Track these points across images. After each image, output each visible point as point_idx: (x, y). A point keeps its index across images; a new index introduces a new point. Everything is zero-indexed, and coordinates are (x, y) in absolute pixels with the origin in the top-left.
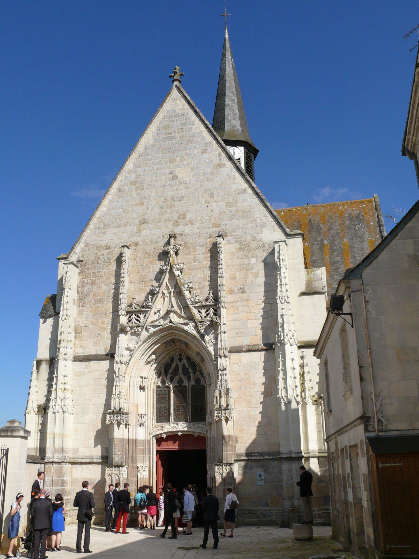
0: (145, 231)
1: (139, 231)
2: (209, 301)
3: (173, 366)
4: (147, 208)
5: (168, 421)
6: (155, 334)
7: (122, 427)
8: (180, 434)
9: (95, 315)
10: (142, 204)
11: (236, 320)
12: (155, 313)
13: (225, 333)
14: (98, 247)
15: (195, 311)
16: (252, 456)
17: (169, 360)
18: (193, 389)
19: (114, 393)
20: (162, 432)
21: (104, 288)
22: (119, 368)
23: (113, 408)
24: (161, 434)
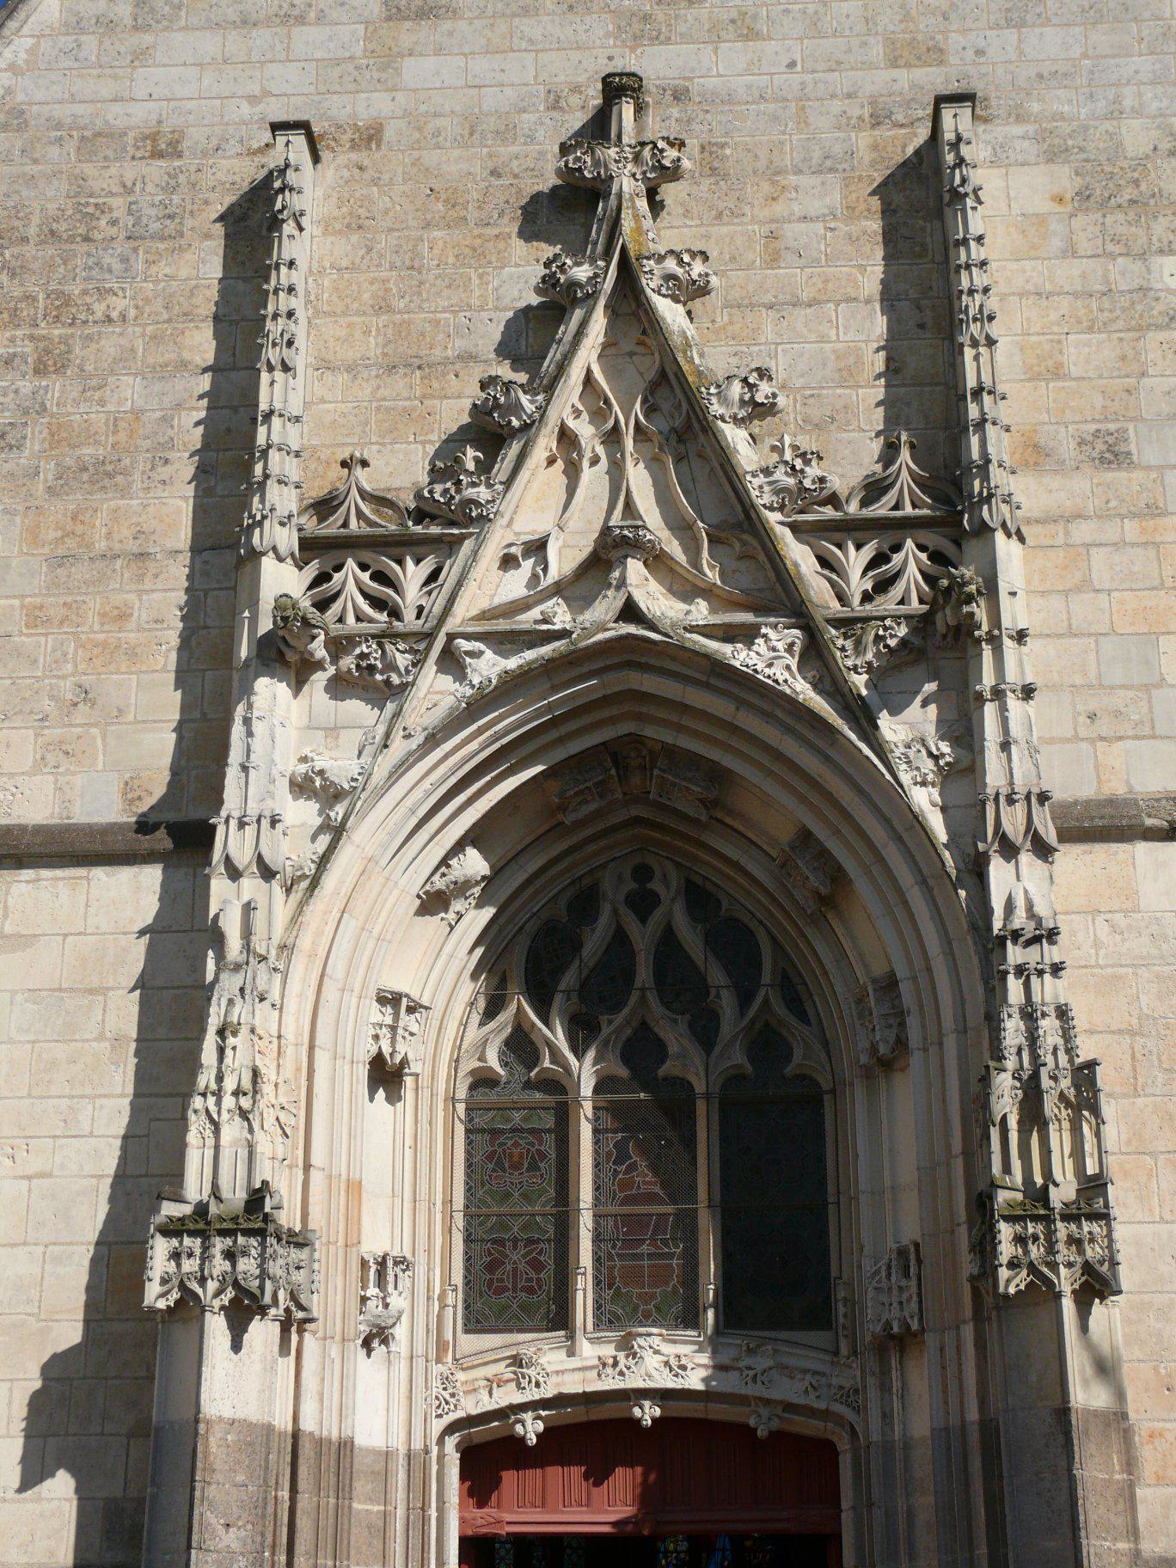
0: (430, 62)
1: (387, 60)
2: (890, 497)
3: (594, 942)
5: (560, 1320)
6: (510, 688)
7: (262, 1332)
8: (648, 1413)
9: (62, 561)
11: (1071, 633)
12: (508, 562)
13: (1028, 692)
14: (95, 141)
15: (799, 556)
17: (563, 902)
18: (735, 1102)
19: (206, 1078)
20: (518, 1398)
21: (129, 391)
22: (248, 908)
23: (195, 1187)
24: (502, 1414)
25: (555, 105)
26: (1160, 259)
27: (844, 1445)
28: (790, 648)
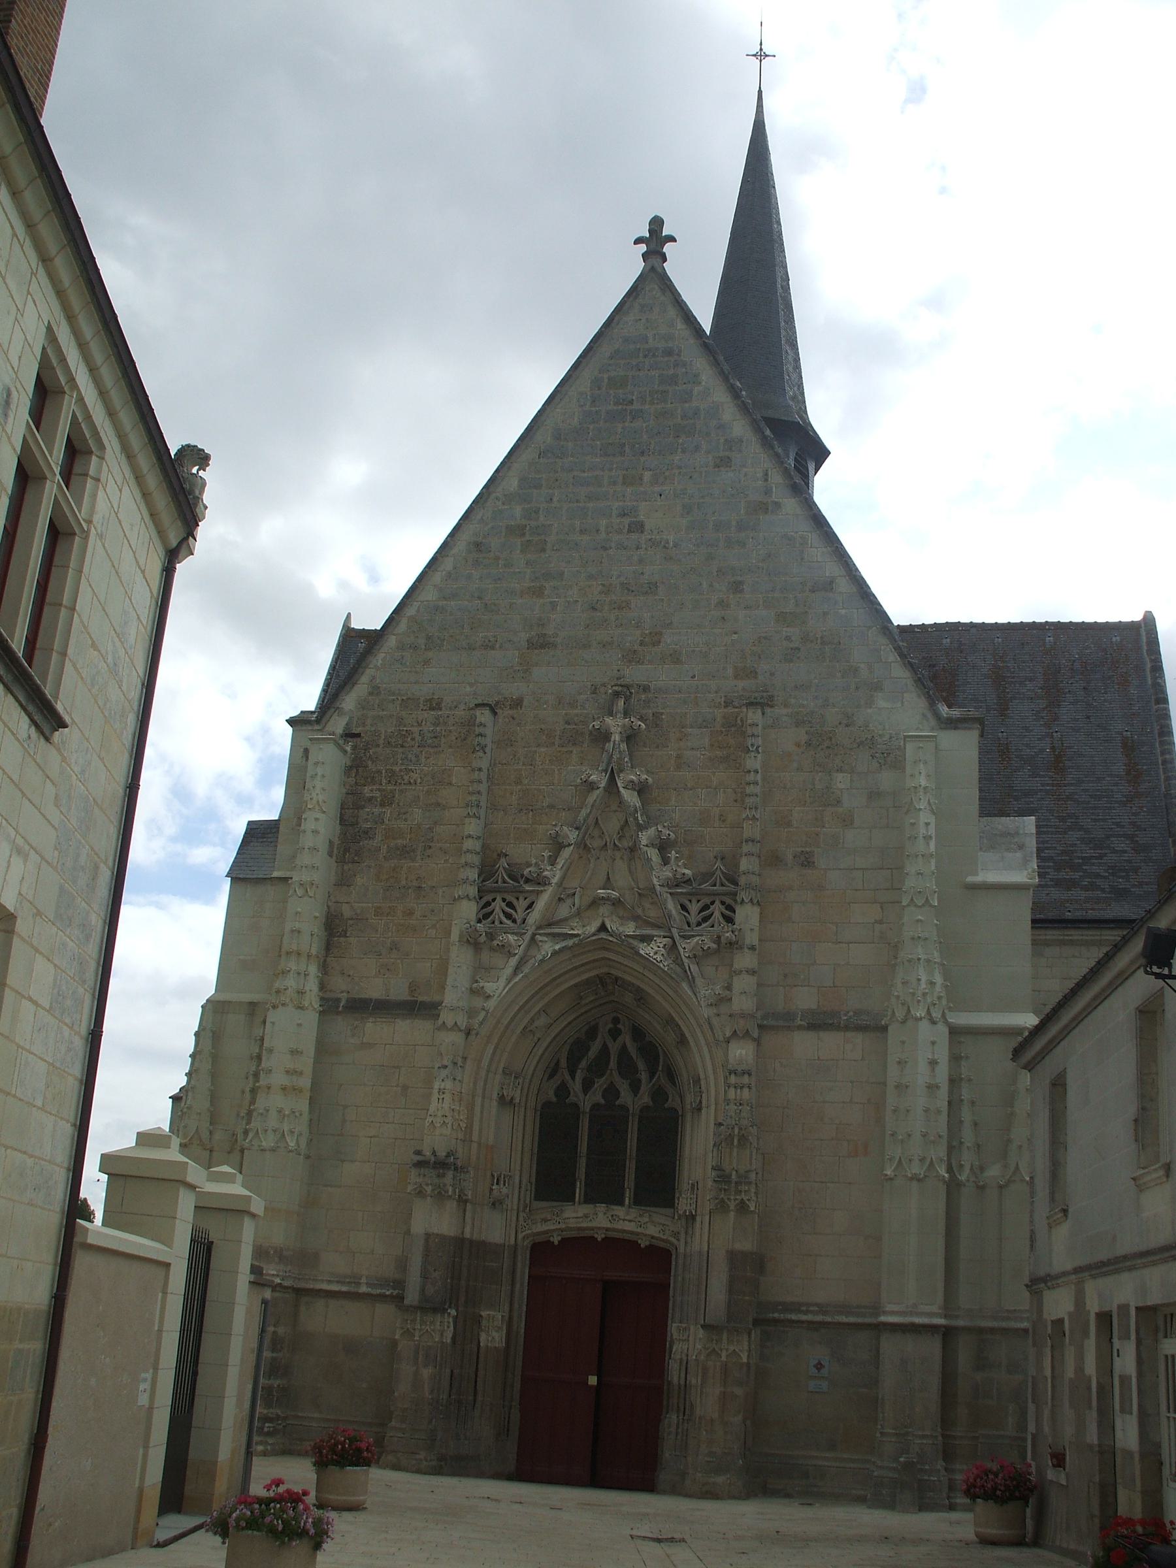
3: (595, 1049)
4: (554, 606)
10: (538, 592)
16: (800, 1311)
25: (594, 692)
26: (835, 774)
27: (674, 1252)
28: (664, 947)
